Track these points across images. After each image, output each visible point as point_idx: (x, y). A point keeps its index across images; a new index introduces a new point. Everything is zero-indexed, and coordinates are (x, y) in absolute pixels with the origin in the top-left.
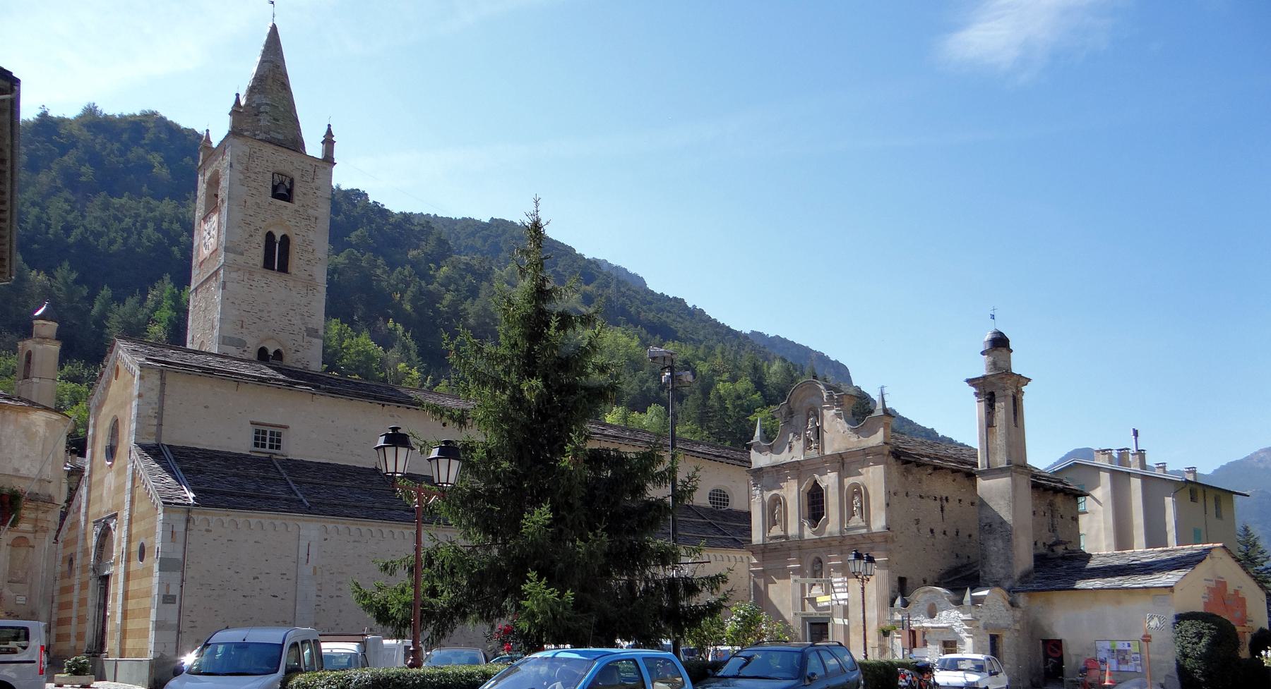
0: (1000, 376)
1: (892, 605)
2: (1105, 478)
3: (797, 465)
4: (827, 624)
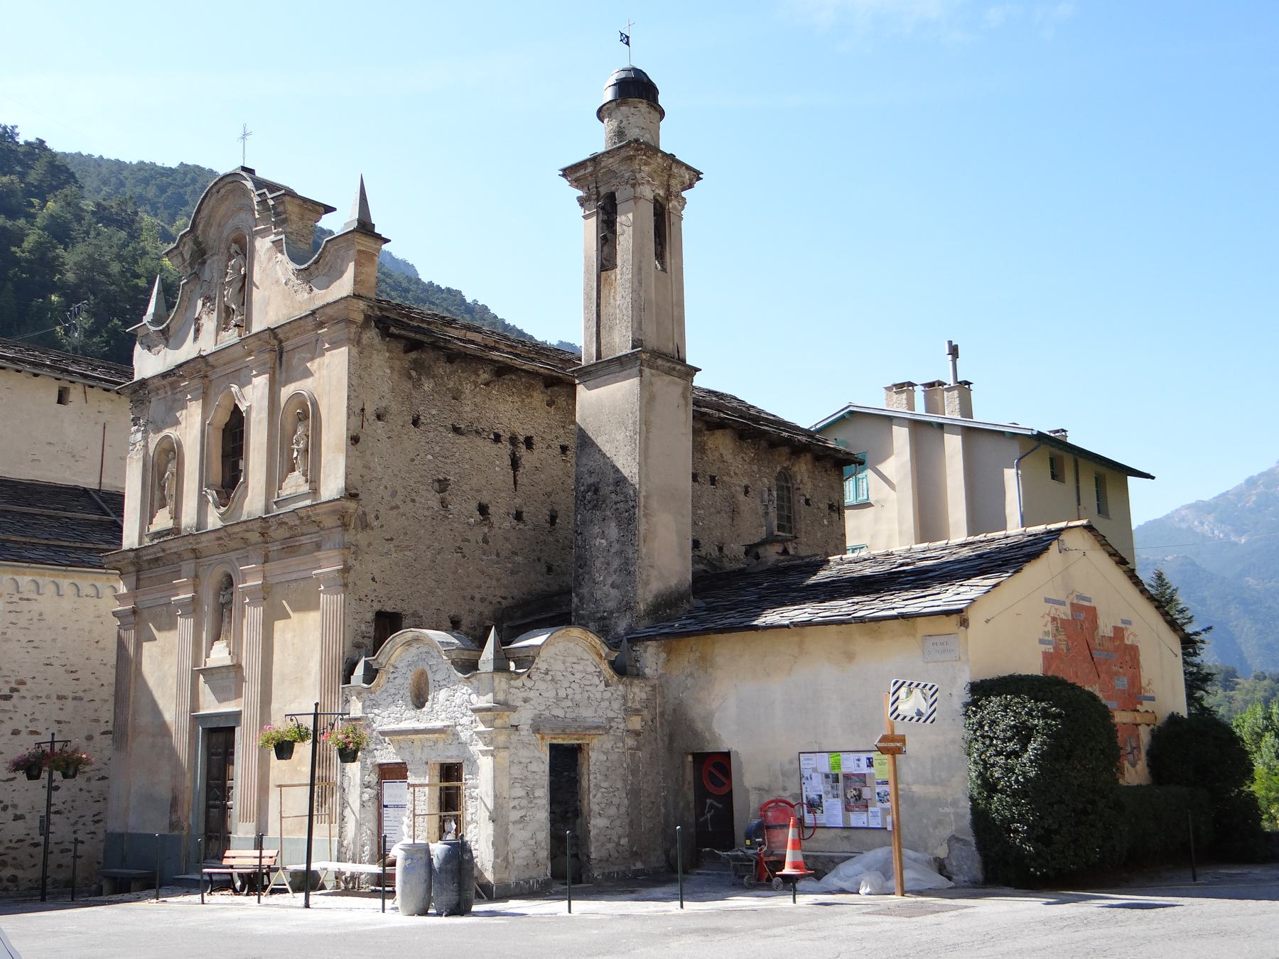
0: (623, 153)
1: (347, 680)
2: (901, 436)
3: (202, 365)
4: (232, 730)
